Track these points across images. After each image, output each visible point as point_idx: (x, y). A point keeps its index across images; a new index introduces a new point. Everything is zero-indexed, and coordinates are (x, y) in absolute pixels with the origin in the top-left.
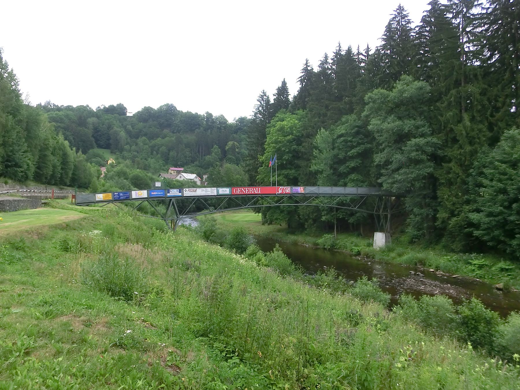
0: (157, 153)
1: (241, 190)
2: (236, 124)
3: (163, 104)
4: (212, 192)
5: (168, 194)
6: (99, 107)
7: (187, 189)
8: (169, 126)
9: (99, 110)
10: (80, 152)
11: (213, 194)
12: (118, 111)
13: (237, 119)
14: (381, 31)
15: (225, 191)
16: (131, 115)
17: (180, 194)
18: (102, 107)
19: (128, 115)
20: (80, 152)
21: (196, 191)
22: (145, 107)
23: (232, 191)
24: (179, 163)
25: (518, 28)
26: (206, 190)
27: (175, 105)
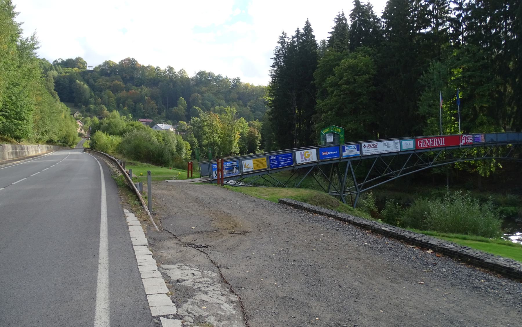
0: (124, 106)
2: (197, 77)
4: (395, 148)
5: (344, 154)
6: (56, 61)
7: (366, 144)
8: (132, 79)
9: (56, 63)
11: (395, 150)
13: (197, 72)
14: (120, 60)
15: (408, 144)
16: (92, 69)
17: (358, 152)
18: (60, 61)
19: (88, 69)
25: (425, 1)
26: (388, 144)
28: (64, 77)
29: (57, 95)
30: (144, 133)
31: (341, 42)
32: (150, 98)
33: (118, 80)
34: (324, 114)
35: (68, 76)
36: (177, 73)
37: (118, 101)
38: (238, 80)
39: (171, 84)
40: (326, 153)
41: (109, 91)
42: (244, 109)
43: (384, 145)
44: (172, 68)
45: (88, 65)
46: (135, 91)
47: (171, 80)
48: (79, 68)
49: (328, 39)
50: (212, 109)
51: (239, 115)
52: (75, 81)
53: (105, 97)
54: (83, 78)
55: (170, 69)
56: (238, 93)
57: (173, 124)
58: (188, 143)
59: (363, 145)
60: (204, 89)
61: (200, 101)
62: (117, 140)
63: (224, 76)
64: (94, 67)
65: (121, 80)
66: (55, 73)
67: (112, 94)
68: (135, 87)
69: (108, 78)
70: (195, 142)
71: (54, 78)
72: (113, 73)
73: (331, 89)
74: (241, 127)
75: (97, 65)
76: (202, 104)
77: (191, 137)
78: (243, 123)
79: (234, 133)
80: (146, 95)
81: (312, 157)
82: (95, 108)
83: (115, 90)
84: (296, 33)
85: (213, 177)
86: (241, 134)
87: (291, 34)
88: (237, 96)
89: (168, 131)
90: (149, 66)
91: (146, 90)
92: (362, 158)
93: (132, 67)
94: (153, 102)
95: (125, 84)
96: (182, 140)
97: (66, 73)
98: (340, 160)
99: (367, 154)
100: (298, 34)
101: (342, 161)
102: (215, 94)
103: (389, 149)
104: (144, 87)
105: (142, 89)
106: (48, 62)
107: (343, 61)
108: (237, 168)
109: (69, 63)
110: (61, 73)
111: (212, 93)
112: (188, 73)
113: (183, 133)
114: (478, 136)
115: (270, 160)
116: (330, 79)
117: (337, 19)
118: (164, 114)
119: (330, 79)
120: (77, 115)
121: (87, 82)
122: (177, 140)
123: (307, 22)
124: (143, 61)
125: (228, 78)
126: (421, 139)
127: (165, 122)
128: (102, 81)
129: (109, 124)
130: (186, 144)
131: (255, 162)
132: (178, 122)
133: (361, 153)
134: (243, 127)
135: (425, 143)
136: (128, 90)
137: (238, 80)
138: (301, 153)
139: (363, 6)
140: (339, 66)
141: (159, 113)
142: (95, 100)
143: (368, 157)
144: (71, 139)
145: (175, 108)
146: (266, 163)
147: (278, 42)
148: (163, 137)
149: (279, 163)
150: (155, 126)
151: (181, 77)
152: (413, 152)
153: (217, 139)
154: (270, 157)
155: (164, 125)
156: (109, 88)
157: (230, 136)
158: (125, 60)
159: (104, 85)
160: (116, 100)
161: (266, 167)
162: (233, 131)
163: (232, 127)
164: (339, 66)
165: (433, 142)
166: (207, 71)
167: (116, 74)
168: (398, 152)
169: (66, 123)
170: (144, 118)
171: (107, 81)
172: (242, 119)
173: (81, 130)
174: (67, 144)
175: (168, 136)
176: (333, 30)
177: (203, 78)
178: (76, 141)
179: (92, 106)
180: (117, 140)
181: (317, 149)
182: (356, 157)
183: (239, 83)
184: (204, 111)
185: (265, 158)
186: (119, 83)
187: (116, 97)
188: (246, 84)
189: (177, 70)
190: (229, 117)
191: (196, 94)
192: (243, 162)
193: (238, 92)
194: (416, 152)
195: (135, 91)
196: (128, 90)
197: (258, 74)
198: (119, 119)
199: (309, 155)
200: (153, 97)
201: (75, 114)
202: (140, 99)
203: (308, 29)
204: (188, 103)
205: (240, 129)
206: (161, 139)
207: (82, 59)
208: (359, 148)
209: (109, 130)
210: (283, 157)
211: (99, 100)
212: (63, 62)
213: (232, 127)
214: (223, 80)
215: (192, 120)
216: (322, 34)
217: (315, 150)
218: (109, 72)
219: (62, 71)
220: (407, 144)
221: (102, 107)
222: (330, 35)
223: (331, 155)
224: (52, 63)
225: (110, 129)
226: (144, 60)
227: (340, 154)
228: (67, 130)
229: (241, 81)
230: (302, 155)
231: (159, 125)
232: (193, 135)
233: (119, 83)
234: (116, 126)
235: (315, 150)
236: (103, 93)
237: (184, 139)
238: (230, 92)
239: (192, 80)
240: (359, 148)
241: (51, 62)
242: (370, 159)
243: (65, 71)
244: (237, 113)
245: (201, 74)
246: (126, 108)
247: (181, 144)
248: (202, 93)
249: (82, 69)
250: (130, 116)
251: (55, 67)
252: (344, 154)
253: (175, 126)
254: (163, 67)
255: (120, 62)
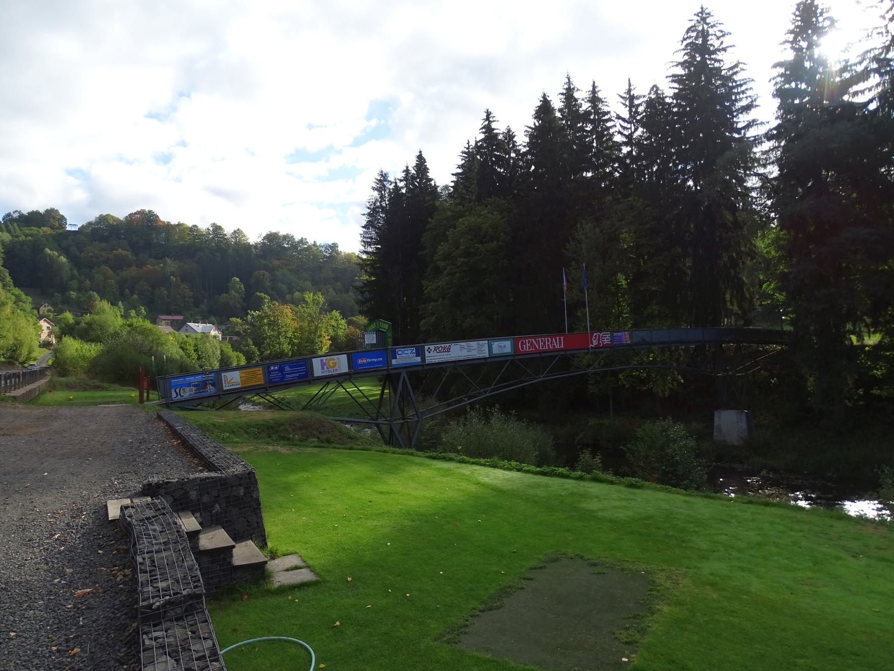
0: (132, 293)
1: (532, 344)
5: (394, 362)
6: (9, 215)
7: (432, 347)
11: (481, 356)
13: (264, 235)
15: (503, 346)
17: (419, 359)
18: (16, 215)
19: (68, 228)
21: (449, 350)
23: (515, 346)
24: (173, 308)
26: (469, 346)
27: (157, 211)
28: (22, 243)
30: (139, 338)
32: (179, 279)
33: (123, 249)
34: (433, 303)
35: (30, 241)
36: (228, 236)
38: (334, 247)
43: (462, 348)
44: (220, 228)
45: (68, 223)
48: (52, 227)
49: (453, 184)
51: (332, 305)
52: (42, 250)
54: (59, 245)
55: (217, 229)
59: (426, 347)
60: (276, 262)
61: (268, 284)
62: (92, 350)
63: (311, 242)
64: (80, 226)
67: (110, 272)
68: (154, 261)
69: (104, 245)
74: (333, 326)
76: (272, 289)
77: (248, 345)
80: (172, 273)
83: (118, 265)
84: (403, 175)
85: (171, 397)
86: (333, 339)
87: (396, 174)
90: (179, 225)
91: (171, 265)
92: (426, 367)
95: (136, 255)
96: (231, 350)
97: (26, 236)
99: (433, 361)
103: (470, 354)
104: (168, 260)
105: (165, 263)
107: (460, 220)
108: (213, 385)
110: (17, 237)
113: (235, 338)
114: (619, 334)
115: (270, 372)
116: (442, 248)
117: (465, 153)
119: (442, 248)
120: (44, 309)
121: (66, 252)
122: (222, 351)
125: (318, 244)
129: (89, 324)
130: (237, 357)
131: (243, 375)
132: (228, 319)
133: (423, 359)
134: (335, 325)
137: (334, 247)
138: (322, 361)
139: (497, 134)
141: (196, 305)
143: (436, 367)
144: (24, 352)
145: (224, 295)
147: (374, 189)
148: (196, 345)
149: (284, 376)
150: (185, 328)
151: (235, 243)
153: (286, 347)
154: (269, 367)
155: (201, 325)
156: (106, 262)
157: (313, 342)
158: (136, 213)
161: (262, 382)
163: (317, 327)
165: (545, 343)
166: (282, 233)
167: (119, 238)
168: (485, 358)
170: (169, 313)
172: (336, 313)
173: (49, 335)
174: (17, 360)
175: (205, 343)
176: (460, 171)
177: (275, 244)
178: (34, 355)
179: (73, 294)
180: (92, 350)
181: (348, 354)
182: (416, 365)
183: (338, 253)
184: (273, 299)
185: (260, 369)
186: (125, 253)
188: (349, 254)
189: (228, 230)
190: (313, 310)
194: (517, 357)
197: (349, 239)
198: (110, 315)
199: (335, 364)
205: (331, 331)
206: (191, 349)
207: (57, 211)
208: (420, 353)
209: (85, 334)
210: (290, 367)
211: (88, 282)
212: (22, 216)
214: (309, 246)
216: (443, 174)
217: (345, 356)
218: (106, 234)
219: (18, 232)
220: (500, 347)
221: (90, 296)
222: (454, 178)
225: (91, 332)
227: (388, 363)
228: (16, 335)
229: (340, 249)
230: (323, 365)
231: (191, 324)
232: (250, 341)
233: (125, 253)
234: (102, 328)
235: (345, 356)
237: (235, 348)
240: (420, 353)
242: (440, 367)
243: (24, 234)
245: (272, 237)
246: (135, 296)
247: (229, 358)
248: (271, 270)
249: (58, 228)
250: (143, 311)
251: (7, 227)
253: (224, 327)
254: (204, 226)
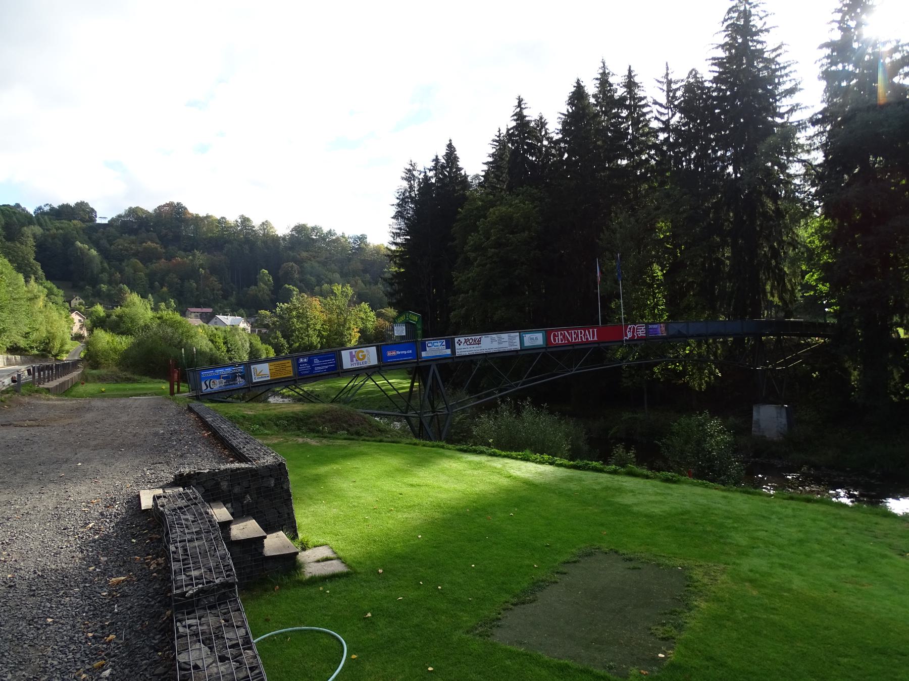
0: (162, 286)
3: (163, 203)
4: (511, 344)
5: (424, 354)
6: (40, 208)
7: (462, 339)
8: (177, 238)
9: (40, 212)
10: (32, 282)
11: (512, 348)
12: (80, 213)
15: (534, 339)
16: (106, 222)
17: (449, 352)
18: (47, 209)
19: (98, 221)
20: (32, 282)
22: (130, 208)
23: (547, 339)
26: (500, 338)
28: (54, 237)
29: (39, 268)
31: (498, 180)
32: (208, 271)
33: (153, 241)
36: (256, 228)
37: (151, 276)
39: (247, 247)
40: (394, 353)
41: (135, 260)
42: (373, 287)
43: (493, 340)
45: (98, 216)
46: (181, 258)
47: (247, 240)
49: (483, 174)
50: (317, 288)
51: (361, 298)
52: (73, 244)
53: (129, 270)
54: (89, 238)
55: (245, 220)
56: (363, 262)
57: (248, 317)
58: (270, 347)
59: (456, 340)
60: (304, 254)
61: (296, 276)
62: (123, 342)
63: (339, 233)
64: (109, 219)
65: (158, 241)
66: (38, 230)
68: (182, 253)
69: (133, 237)
70: (282, 346)
71: (35, 238)
72: (143, 229)
73: (474, 255)
74: (362, 319)
75: (114, 216)
77: (277, 338)
78: (366, 312)
79: (349, 328)
80: (201, 266)
81: (369, 359)
82: (109, 290)
83: (147, 257)
84: (433, 164)
88: (360, 266)
89: (234, 328)
90: (208, 217)
92: (456, 360)
93: (177, 219)
94: (213, 278)
95: (165, 247)
96: (260, 343)
97: (58, 229)
98: (417, 362)
100: (436, 164)
101: (421, 364)
102: (324, 264)
103: (501, 346)
106: (24, 210)
108: (242, 377)
109: (63, 213)
110: (48, 230)
111: (319, 262)
112: (276, 228)
113: (264, 331)
115: (299, 365)
116: (473, 239)
117: (496, 141)
118: (233, 299)
119: (473, 239)
120: (75, 302)
121: (96, 245)
122: (251, 344)
123: (450, 146)
124: (196, 207)
125: (346, 236)
126: (557, 330)
127: (234, 313)
128: (123, 242)
132: (257, 312)
133: (453, 352)
135: (564, 337)
136: (169, 258)
137: (362, 238)
138: (351, 353)
139: (529, 122)
140: (486, 218)
141: (225, 297)
142: (111, 275)
144: (57, 344)
145: (253, 287)
146: (291, 368)
147: (403, 178)
148: (225, 338)
149: (313, 368)
150: (214, 320)
151: (264, 235)
152: (543, 350)
153: (315, 340)
154: (298, 360)
156: (136, 254)
157: (342, 335)
158: (164, 206)
159: (127, 250)
160: (146, 275)
161: (292, 375)
162: (347, 325)
163: (345, 319)
164: (486, 218)
165: (577, 336)
166: (310, 224)
167: (148, 231)
168: (517, 351)
169: (47, 317)
171: (133, 242)
174: (50, 352)
175: (234, 335)
176: (491, 160)
177: (303, 238)
178: (67, 347)
179: (104, 287)
181: (377, 347)
182: (445, 358)
184: (301, 291)
186: (154, 245)
187: (148, 271)
189: (256, 222)
190: (342, 302)
191: (291, 264)
192: (252, 367)
193: (364, 260)
194: (549, 350)
195: (181, 258)
196: (169, 258)
198: (140, 308)
199: (364, 356)
200: (213, 270)
201: (74, 302)
202: (190, 273)
203: (451, 155)
204: (276, 279)
205: (360, 323)
206: (221, 341)
207: (87, 204)
208: (450, 345)
209: (116, 326)
210: (320, 359)
211: (118, 275)
212: (52, 209)
213: (345, 319)
214: (338, 239)
215: (278, 309)
216: (474, 164)
217: (374, 348)
222: (486, 168)
223: (403, 355)
224: (32, 213)
226: (198, 206)
227: (418, 356)
228: (49, 328)
230: (352, 357)
231: (220, 317)
232: (279, 334)
233: (154, 245)
234: (132, 321)
235: (374, 348)
236: (124, 264)
238: (349, 260)
239: (284, 239)
240: (450, 345)
241: (31, 210)
242: (470, 360)
243: (56, 227)
244: (353, 296)
246: (165, 289)
247: (258, 350)
250: (173, 304)
252: (424, 354)
253: (253, 320)
254: (232, 218)
255: (155, 210)
